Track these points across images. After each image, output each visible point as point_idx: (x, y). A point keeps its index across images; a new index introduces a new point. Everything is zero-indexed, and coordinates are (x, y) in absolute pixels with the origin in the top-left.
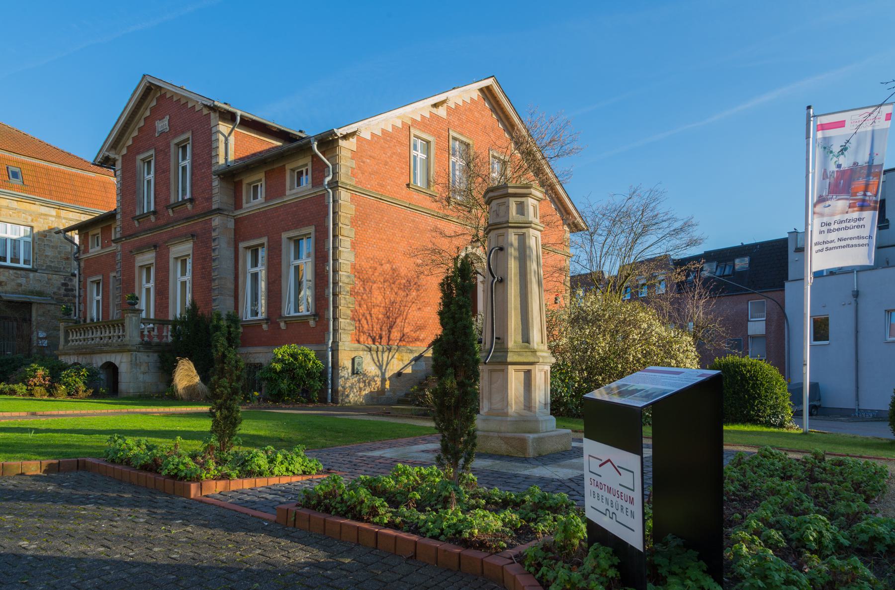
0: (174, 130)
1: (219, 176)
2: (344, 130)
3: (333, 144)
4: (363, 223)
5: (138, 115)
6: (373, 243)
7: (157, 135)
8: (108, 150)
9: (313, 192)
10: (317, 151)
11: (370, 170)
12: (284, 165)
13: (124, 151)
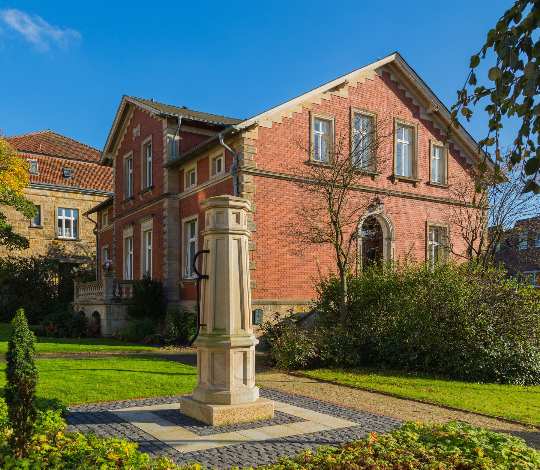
0: (143, 135)
1: (167, 167)
2: (244, 124)
3: (238, 137)
4: (264, 199)
5: (123, 125)
6: (274, 214)
7: (134, 139)
8: (106, 154)
9: (225, 176)
10: (224, 144)
11: (271, 153)
12: (209, 156)
13: (117, 153)
